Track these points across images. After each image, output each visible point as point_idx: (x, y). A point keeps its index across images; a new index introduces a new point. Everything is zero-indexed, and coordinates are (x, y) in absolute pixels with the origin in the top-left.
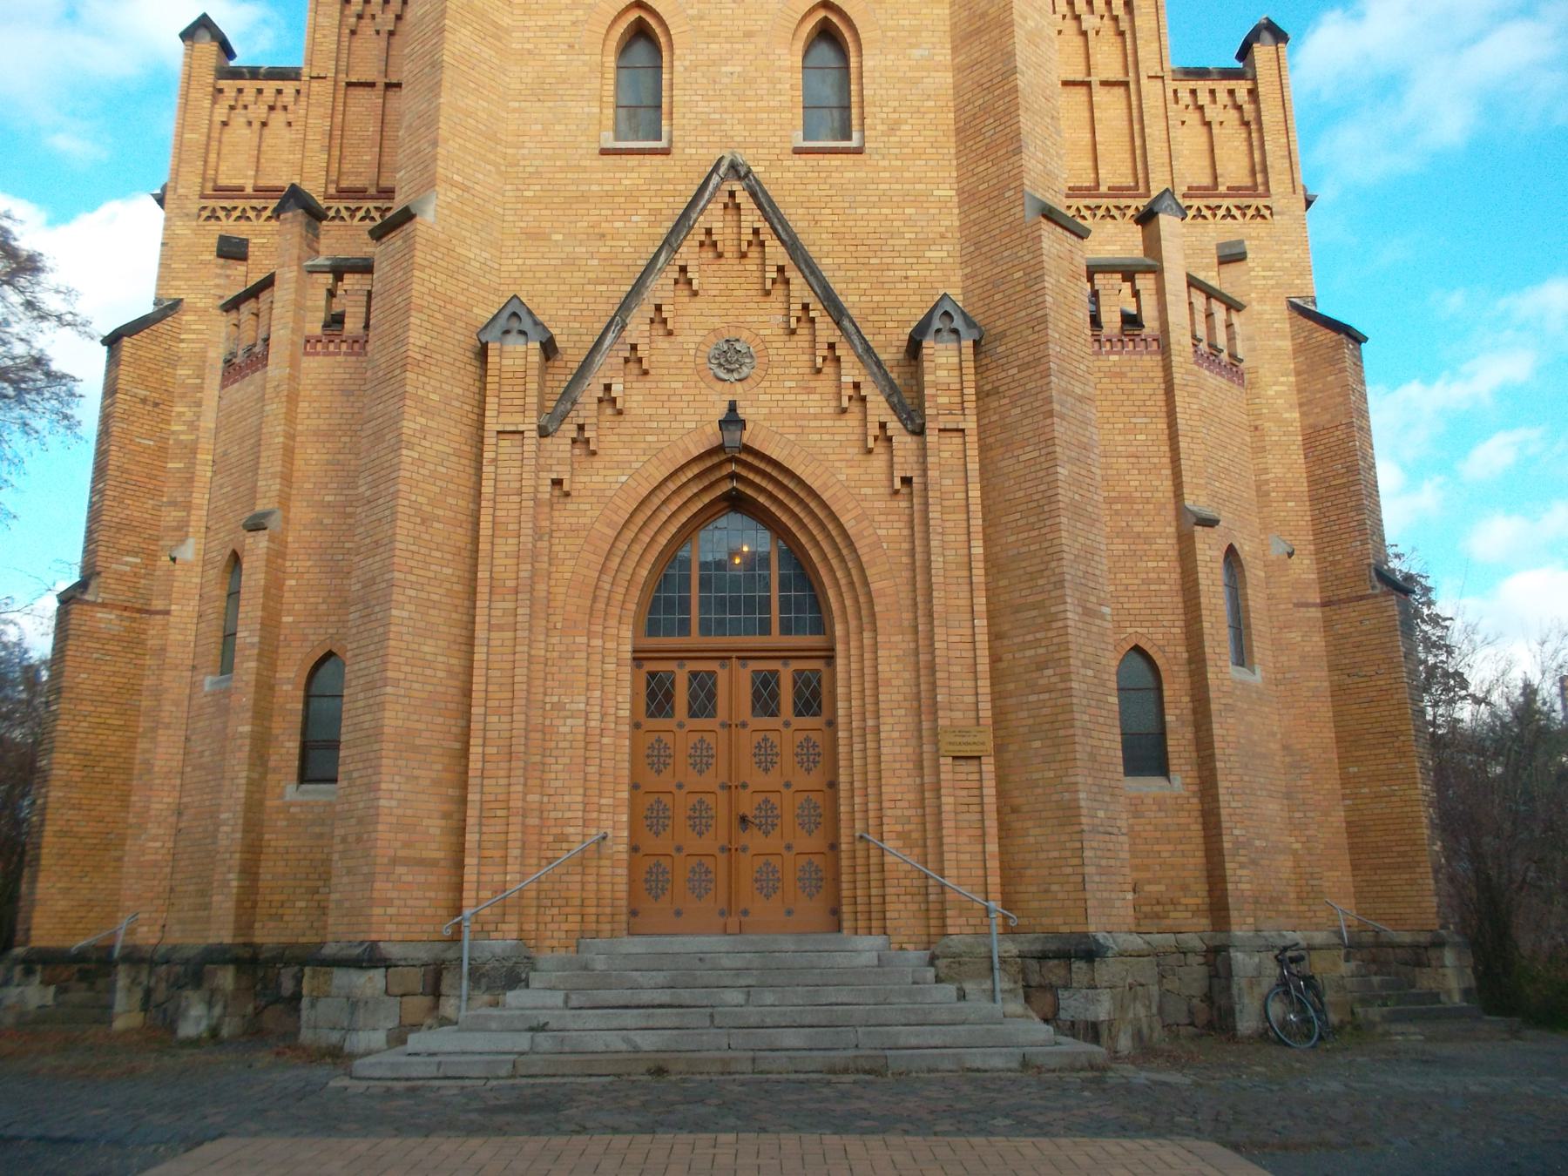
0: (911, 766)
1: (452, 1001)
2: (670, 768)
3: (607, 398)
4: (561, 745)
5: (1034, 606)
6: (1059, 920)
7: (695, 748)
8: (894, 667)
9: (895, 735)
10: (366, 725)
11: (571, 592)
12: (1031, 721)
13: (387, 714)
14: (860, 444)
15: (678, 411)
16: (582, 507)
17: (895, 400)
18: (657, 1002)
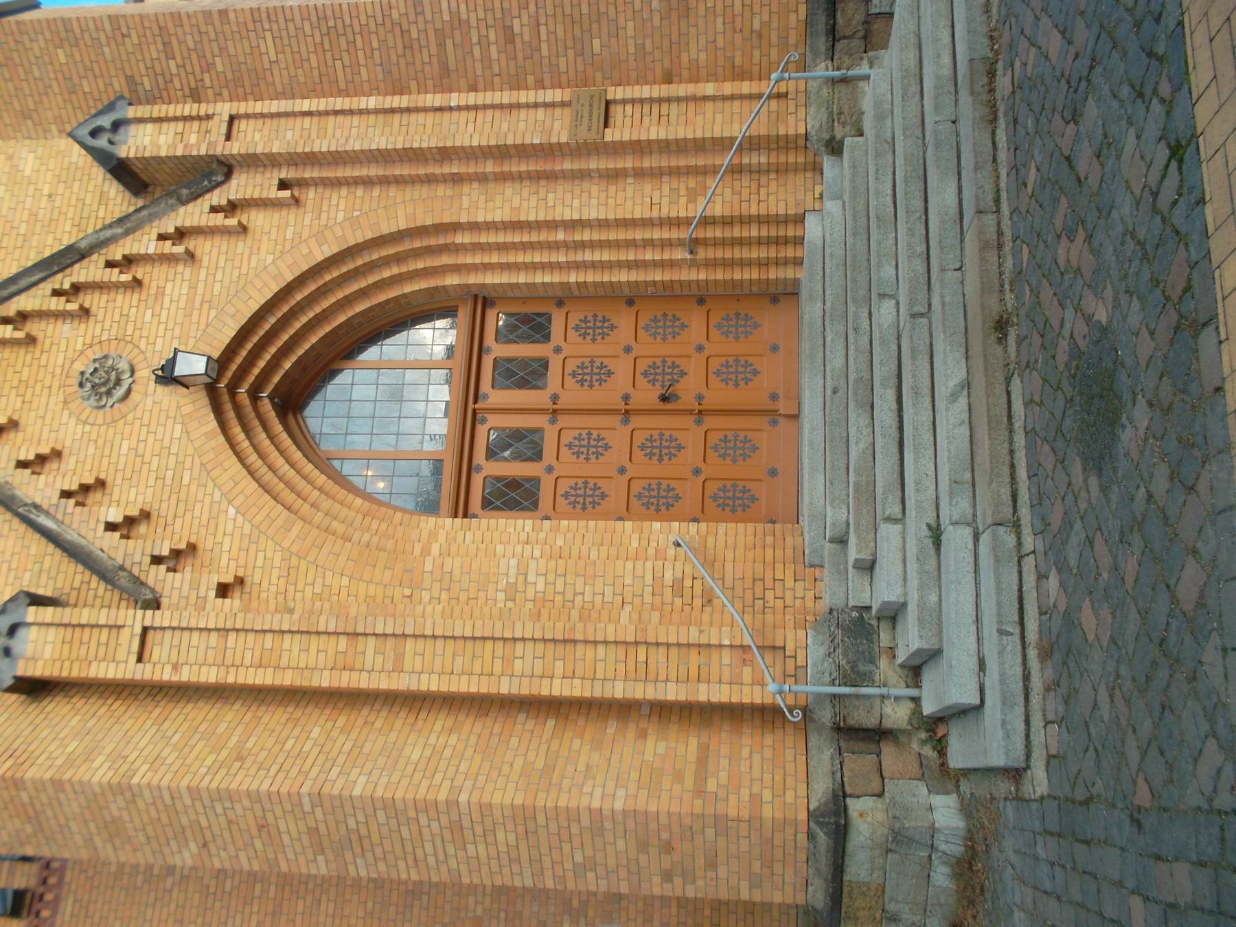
0: (612, 189)
1: (888, 709)
2: (600, 483)
3: (126, 526)
4: (560, 588)
5: (442, 45)
6: (793, 17)
7: (578, 454)
8: (498, 204)
9: (576, 203)
10: (512, 838)
11: (366, 577)
12: (571, 53)
13: (496, 800)
14: (233, 240)
15: (158, 444)
16: (260, 563)
17: (185, 192)
18: (894, 406)
